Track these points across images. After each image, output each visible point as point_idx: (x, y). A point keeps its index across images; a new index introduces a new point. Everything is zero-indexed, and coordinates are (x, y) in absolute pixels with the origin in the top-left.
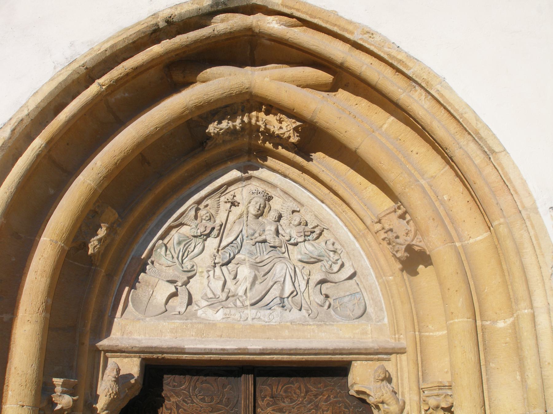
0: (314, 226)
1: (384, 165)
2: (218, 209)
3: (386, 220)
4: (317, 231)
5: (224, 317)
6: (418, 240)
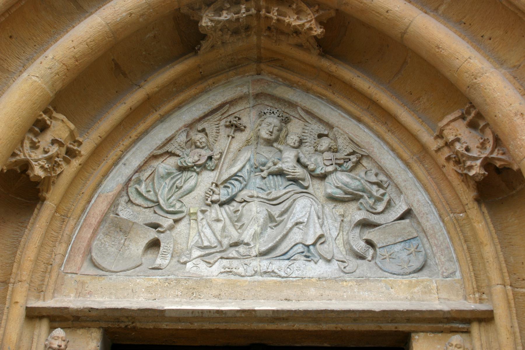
0: (348, 153)
1: (443, 49)
2: (218, 134)
3: (451, 129)
4: (354, 158)
5: (223, 270)
6: (501, 152)
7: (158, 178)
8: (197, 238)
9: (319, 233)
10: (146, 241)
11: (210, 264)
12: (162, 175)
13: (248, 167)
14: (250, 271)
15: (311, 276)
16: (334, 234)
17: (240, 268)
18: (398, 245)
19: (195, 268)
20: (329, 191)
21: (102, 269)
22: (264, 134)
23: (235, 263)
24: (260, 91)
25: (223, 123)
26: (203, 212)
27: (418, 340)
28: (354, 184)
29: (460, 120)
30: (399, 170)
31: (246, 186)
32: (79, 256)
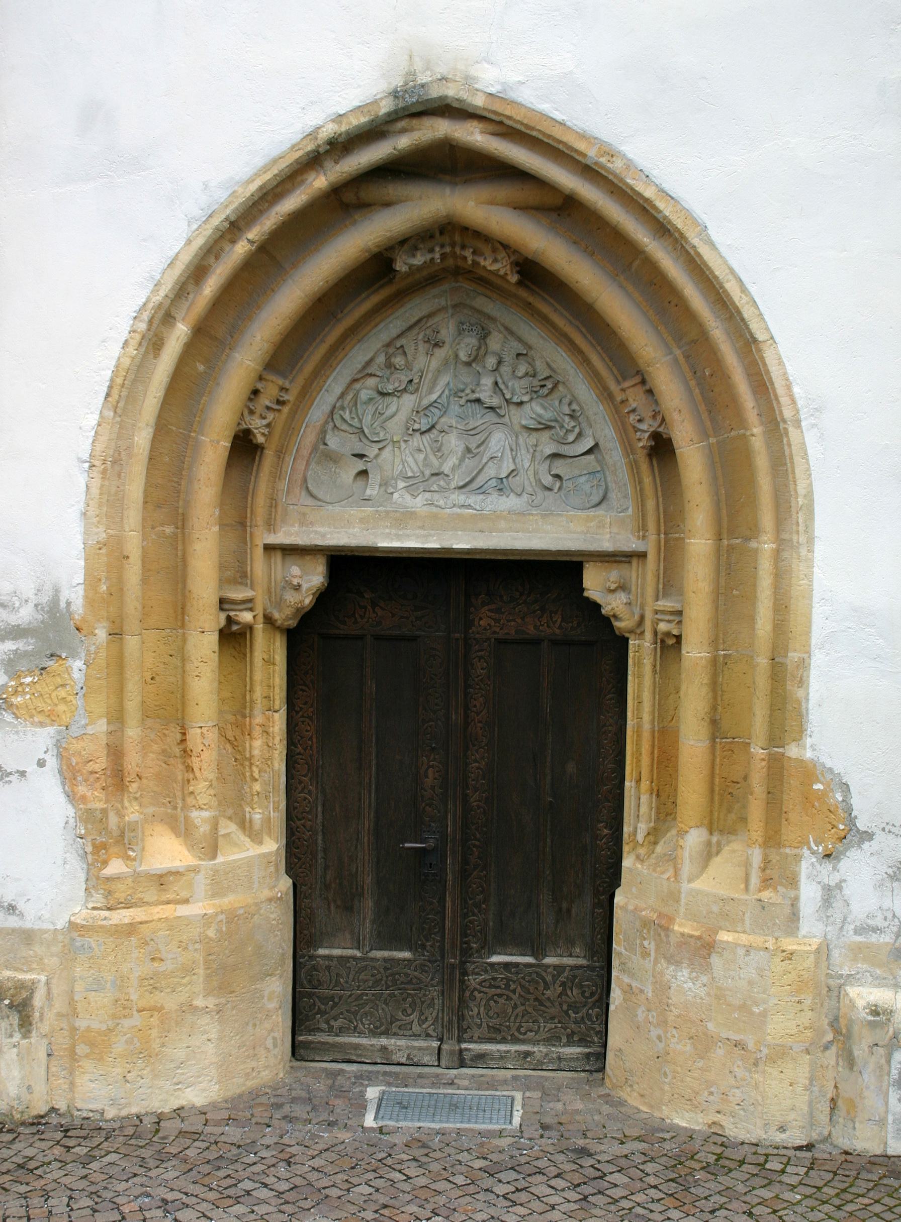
4: (550, 385)
9: (512, 467)
10: (356, 471)
11: (415, 497)
13: (447, 392)
14: (450, 504)
16: (527, 465)
20: (524, 422)
21: (319, 500)
22: (463, 356)
23: (436, 496)
25: (421, 337)
26: (406, 441)
28: (547, 415)
29: (640, 386)
31: (445, 412)
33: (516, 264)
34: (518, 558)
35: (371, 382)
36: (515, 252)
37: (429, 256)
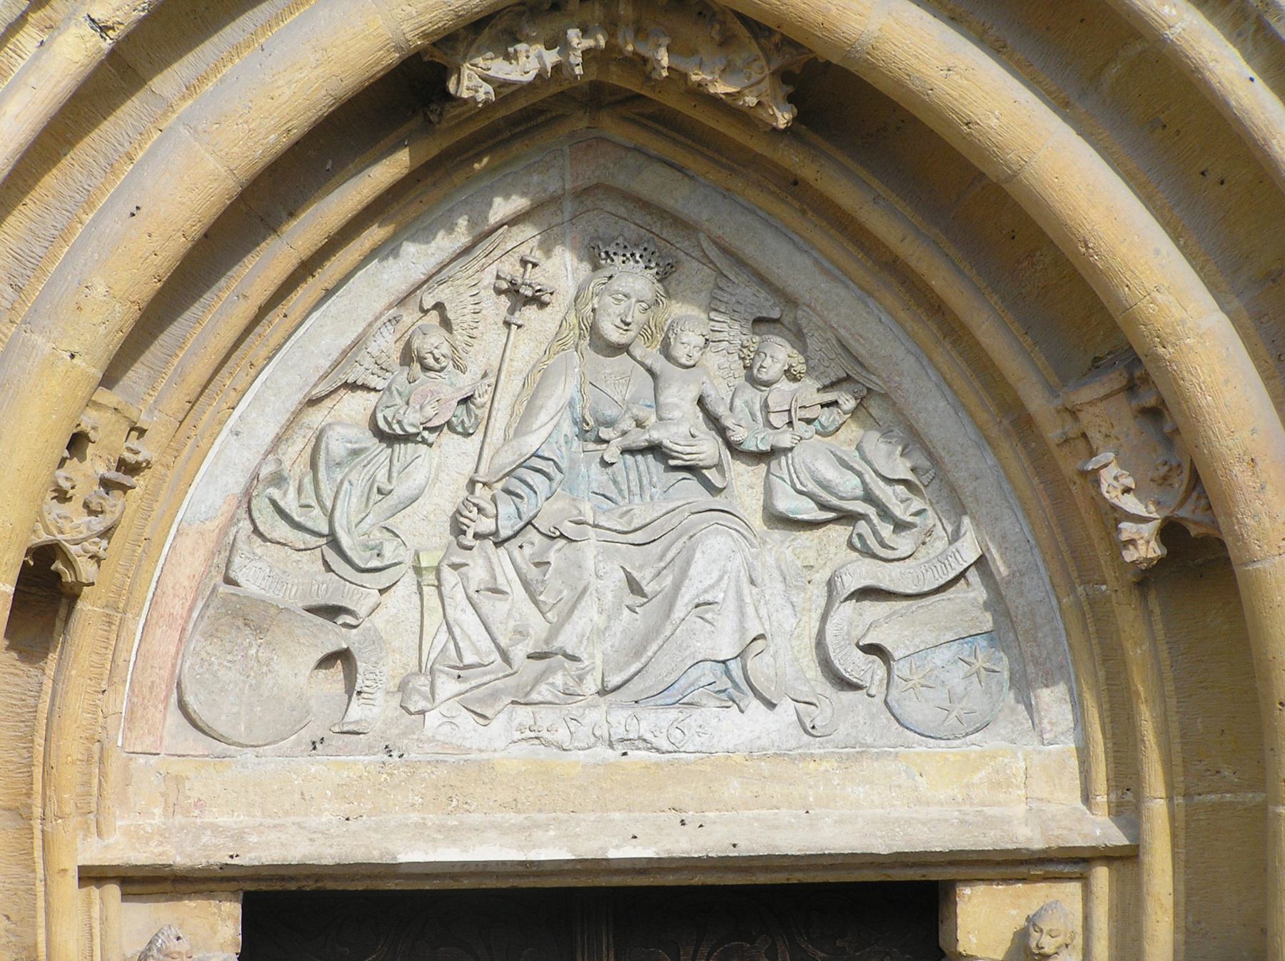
5: (518, 735)
7: (328, 468)
8: (443, 636)
12: (338, 460)
15: (731, 748)
17: (560, 730)
18: (944, 649)
19: (447, 728)
23: (546, 717)
24: (595, 181)
26: (455, 567)
27: (970, 897)
30: (962, 446)
32: (156, 707)
33: (784, 76)
34: (779, 878)
35: (355, 406)
36: (789, 43)
37: (551, 57)
